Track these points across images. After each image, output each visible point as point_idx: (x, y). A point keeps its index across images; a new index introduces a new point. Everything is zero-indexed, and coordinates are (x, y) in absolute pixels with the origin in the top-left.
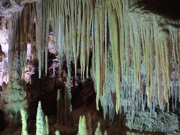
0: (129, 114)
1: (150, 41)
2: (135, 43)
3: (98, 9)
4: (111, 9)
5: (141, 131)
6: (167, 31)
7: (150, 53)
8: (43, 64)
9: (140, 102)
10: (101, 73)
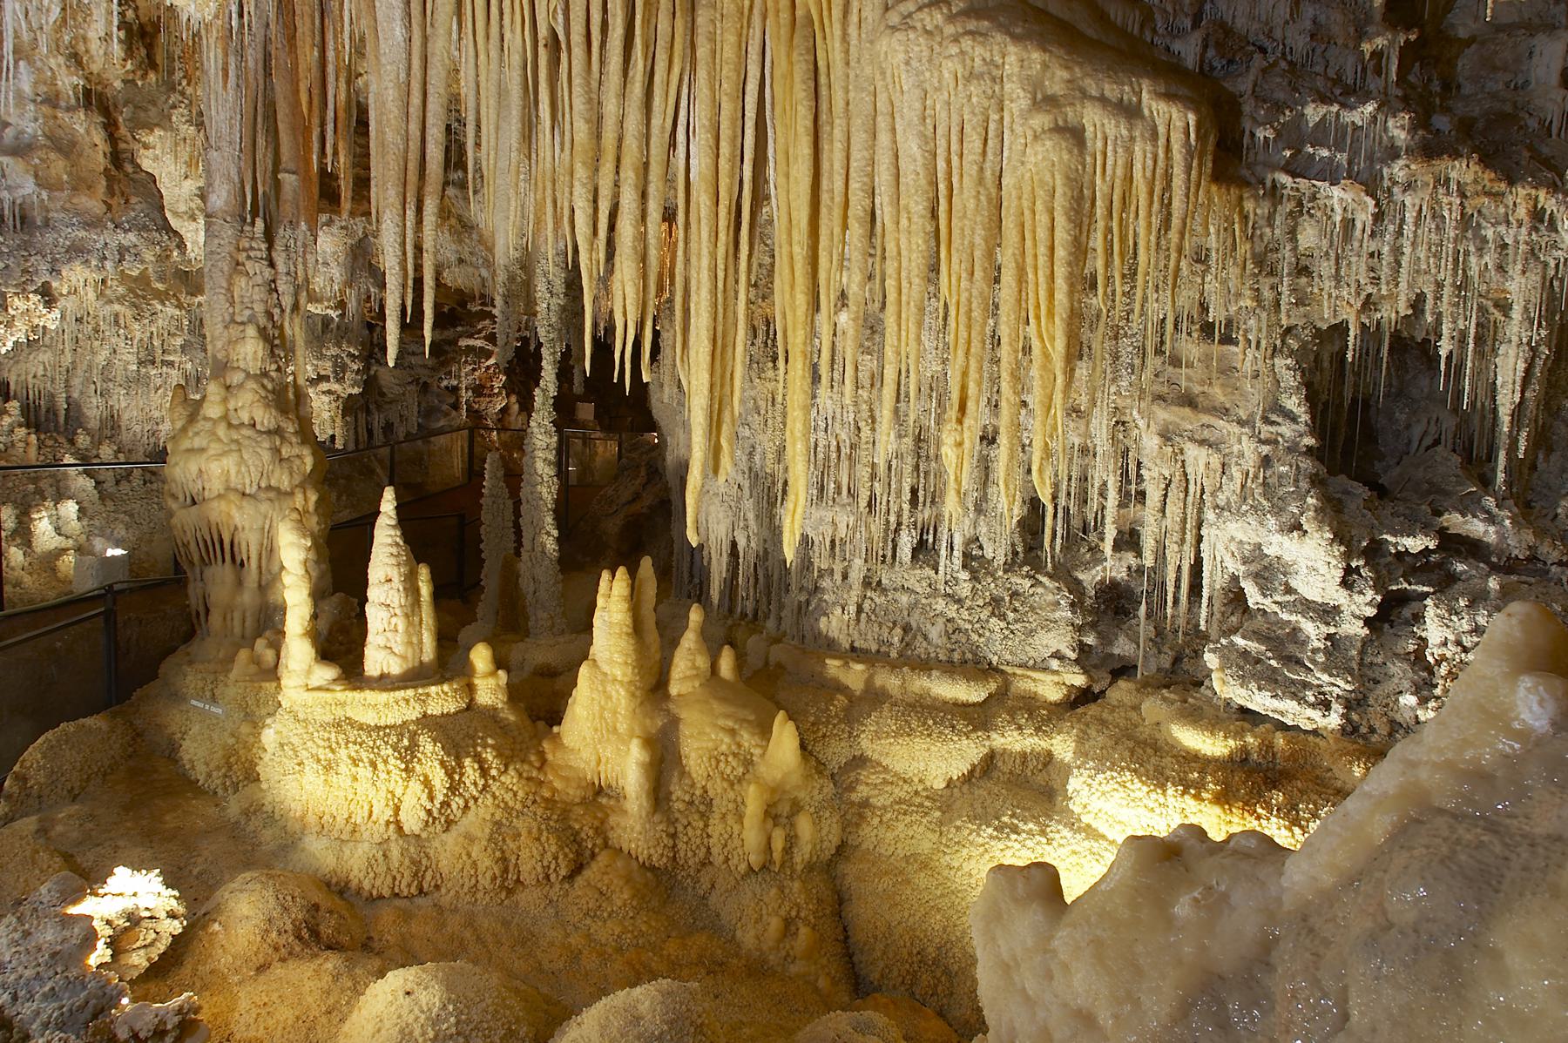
0: (838, 577)
1: (981, 190)
2: (902, 202)
3: (718, 16)
4: (785, 16)
5: (894, 654)
6: (1076, 135)
7: (978, 254)
8: (410, 290)
9: (893, 518)
10: (718, 363)
